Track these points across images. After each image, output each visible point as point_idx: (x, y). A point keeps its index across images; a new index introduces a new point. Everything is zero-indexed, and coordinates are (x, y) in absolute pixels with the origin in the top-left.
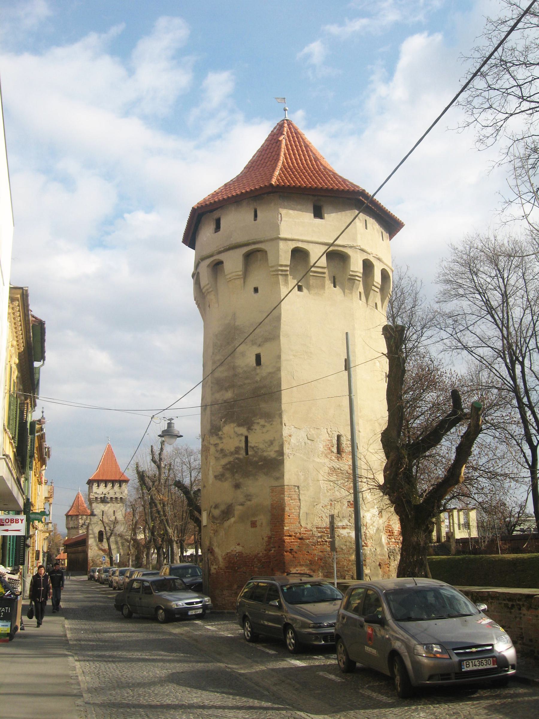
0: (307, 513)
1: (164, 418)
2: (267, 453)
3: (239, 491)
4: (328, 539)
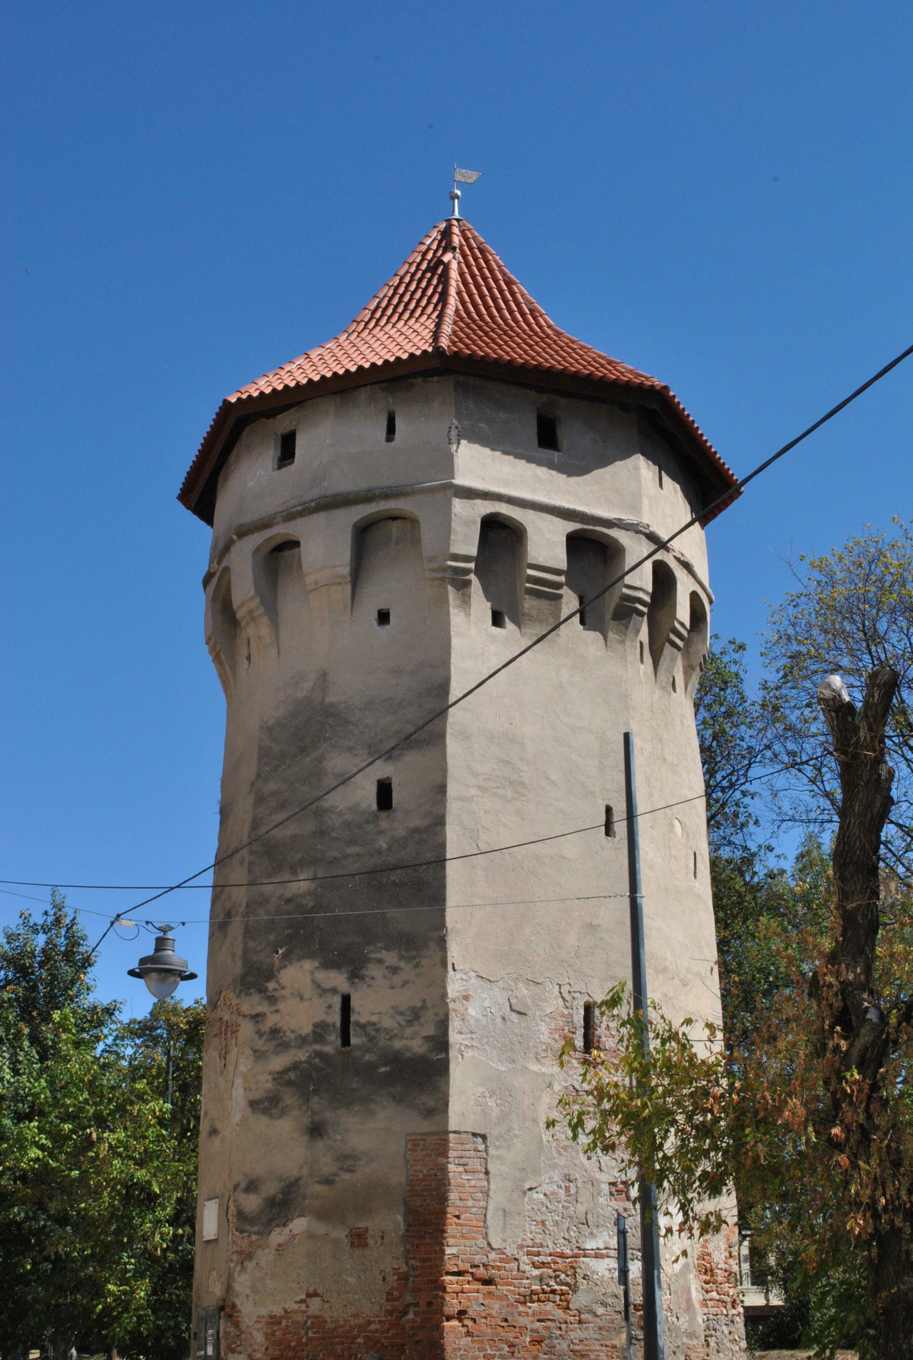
0: (504, 1211)
1: (147, 923)
2: (404, 1042)
3: (320, 1144)
4: (558, 1284)
